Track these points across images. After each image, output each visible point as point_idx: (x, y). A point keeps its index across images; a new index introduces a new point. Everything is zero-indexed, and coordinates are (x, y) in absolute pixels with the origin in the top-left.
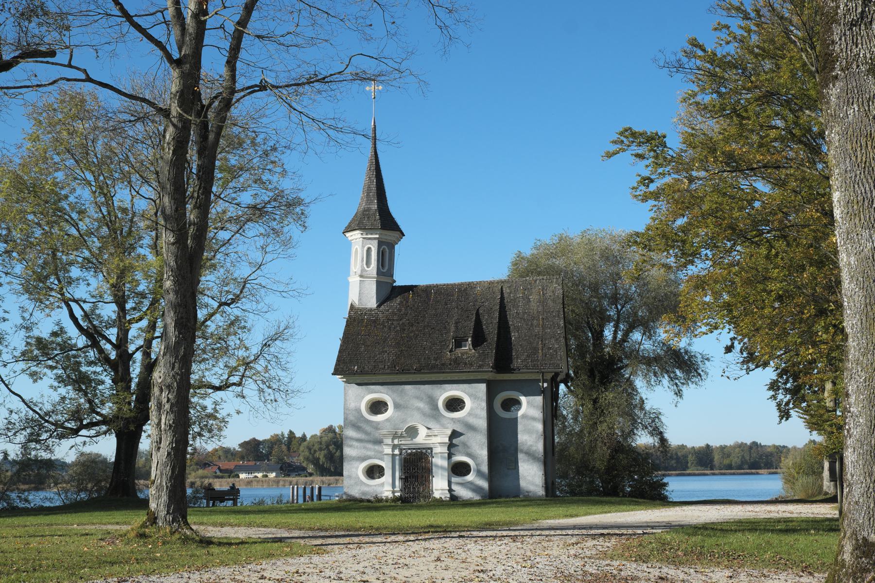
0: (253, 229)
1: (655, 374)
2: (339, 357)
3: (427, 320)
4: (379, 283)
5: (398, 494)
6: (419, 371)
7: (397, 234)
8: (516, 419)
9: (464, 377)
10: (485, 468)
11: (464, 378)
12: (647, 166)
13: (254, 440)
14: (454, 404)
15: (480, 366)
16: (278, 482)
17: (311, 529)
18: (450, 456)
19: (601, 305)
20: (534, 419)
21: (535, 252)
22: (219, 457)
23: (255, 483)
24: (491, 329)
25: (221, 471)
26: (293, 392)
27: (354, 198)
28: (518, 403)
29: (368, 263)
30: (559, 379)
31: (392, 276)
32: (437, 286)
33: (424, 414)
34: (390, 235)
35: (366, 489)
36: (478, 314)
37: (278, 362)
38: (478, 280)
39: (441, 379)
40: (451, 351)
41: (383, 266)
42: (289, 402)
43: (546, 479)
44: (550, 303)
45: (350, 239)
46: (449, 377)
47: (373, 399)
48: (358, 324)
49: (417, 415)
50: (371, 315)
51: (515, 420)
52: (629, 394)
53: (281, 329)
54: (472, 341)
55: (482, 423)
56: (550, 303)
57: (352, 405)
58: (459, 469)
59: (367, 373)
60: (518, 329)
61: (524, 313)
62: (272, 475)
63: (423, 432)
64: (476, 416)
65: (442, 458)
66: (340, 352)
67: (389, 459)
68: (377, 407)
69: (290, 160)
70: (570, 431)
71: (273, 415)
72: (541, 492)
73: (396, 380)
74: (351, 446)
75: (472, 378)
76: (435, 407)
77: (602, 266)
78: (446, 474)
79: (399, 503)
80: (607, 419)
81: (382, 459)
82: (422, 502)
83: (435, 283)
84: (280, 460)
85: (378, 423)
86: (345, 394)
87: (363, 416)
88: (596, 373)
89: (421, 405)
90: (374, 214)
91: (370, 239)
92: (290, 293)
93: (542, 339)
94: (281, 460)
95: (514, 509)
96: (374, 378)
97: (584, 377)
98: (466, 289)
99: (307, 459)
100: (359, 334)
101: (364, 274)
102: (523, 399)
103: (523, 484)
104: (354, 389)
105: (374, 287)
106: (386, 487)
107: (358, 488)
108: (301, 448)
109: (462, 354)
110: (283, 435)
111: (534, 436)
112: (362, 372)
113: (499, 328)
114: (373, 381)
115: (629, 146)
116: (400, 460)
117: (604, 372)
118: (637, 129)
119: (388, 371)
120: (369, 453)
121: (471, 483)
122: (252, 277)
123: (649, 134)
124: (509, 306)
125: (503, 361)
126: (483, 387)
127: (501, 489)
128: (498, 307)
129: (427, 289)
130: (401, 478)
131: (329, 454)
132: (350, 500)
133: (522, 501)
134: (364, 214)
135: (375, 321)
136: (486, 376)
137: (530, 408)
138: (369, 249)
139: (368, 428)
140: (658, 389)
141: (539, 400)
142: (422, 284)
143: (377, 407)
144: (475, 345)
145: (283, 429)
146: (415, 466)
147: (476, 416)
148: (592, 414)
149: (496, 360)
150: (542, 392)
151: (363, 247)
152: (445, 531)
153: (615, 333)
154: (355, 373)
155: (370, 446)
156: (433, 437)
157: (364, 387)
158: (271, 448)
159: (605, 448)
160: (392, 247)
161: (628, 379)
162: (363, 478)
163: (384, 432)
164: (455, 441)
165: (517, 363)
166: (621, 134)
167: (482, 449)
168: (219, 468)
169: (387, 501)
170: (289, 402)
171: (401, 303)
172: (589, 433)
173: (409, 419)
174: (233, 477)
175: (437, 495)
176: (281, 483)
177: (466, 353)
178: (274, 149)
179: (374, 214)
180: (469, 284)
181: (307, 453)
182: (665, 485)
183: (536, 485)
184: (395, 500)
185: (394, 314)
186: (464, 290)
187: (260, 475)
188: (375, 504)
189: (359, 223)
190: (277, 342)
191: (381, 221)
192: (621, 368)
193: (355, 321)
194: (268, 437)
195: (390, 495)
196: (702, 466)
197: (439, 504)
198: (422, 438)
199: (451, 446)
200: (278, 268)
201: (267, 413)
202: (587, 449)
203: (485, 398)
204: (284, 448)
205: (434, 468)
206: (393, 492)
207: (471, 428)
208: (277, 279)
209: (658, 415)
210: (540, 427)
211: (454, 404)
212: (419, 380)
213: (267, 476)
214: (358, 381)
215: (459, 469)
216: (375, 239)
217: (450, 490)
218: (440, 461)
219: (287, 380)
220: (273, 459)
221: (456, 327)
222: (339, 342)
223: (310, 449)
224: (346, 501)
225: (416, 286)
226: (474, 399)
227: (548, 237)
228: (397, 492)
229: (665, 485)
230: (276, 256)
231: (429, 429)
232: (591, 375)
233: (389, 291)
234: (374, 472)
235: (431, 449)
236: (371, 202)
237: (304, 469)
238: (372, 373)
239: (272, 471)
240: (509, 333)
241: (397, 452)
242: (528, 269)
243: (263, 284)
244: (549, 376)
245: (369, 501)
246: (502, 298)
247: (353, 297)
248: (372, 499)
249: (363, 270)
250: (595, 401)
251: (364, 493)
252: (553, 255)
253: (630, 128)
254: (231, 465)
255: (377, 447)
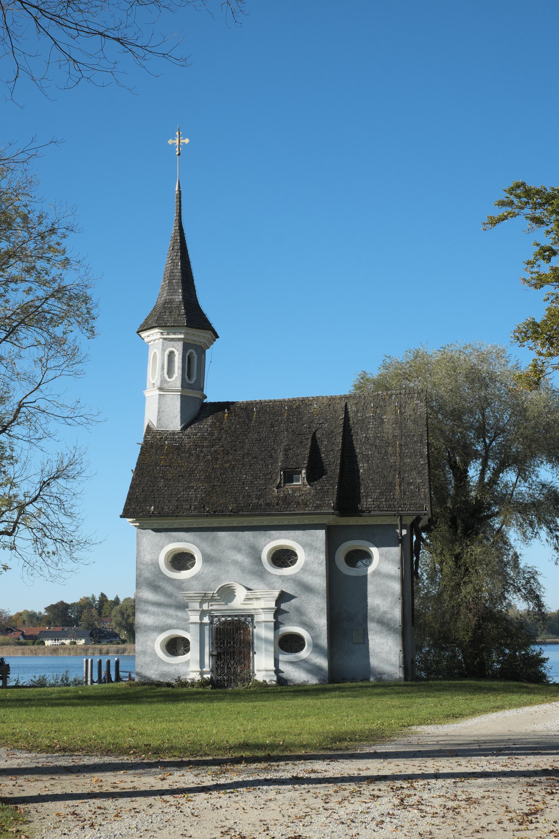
0: (28, 335)
1: (531, 525)
2: (129, 494)
3: (247, 446)
4: (184, 399)
5: (207, 676)
6: (235, 513)
7: (208, 334)
8: (366, 576)
9: (296, 521)
10: (324, 642)
11: (296, 523)
12: (548, 232)
13: (62, 603)
14: (283, 558)
15: (317, 507)
16: (87, 650)
17: (50, 749)
18: (277, 626)
19: (464, 436)
20: (390, 577)
21: (383, 371)
22: (24, 622)
23: (61, 651)
24: (332, 458)
25: (24, 637)
26: (79, 543)
27: (153, 286)
28: (368, 556)
29: (170, 372)
30: (420, 525)
31: (202, 389)
32: (261, 402)
33: (243, 569)
34: (199, 336)
35: (166, 669)
36: (314, 439)
37: (61, 505)
38: (315, 395)
39: (266, 523)
40: (278, 487)
41: (190, 377)
42: (74, 555)
43: (405, 657)
44: (410, 424)
45: (146, 340)
46: (276, 521)
47: (175, 550)
48: (155, 449)
49: (234, 571)
50: (173, 439)
51: (364, 579)
52: (499, 549)
53: (65, 464)
54: (307, 473)
55: (320, 582)
56: (410, 424)
57: (147, 558)
58: (289, 644)
59: (167, 515)
60: (367, 459)
61: (376, 438)
62: (82, 642)
63: (241, 593)
64: (313, 573)
65: (267, 627)
66: (131, 487)
67: (195, 629)
68: (181, 560)
69: (72, 245)
70: (426, 594)
71: (53, 571)
72: (399, 673)
73: (205, 525)
74: (146, 612)
75: (306, 522)
76: (258, 560)
77: (466, 390)
78: (272, 649)
79: (209, 688)
80: (473, 579)
81: (187, 630)
82: (240, 687)
83: (258, 399)
84: (90, 625)
85: (181, 582)
86: (138, 544)
87: (162, 573)
88: (459, 522)
89: (239, 557)
90: (178, 308)
91: (172, 340)
92: (77, 419)
93: (399, 476)
94: (91, 625)
95: (365, 700)
96: (177, 522)
97: (443, 528)
98: (298, 407)
99: (119, 624)
100: (157, 465)
101: (166, 386)
102: (374, 551)
103: (374, 662)
104: (150, 536)
105: (178, 403)
106: (192, 666)
107: (155, 667)
108: (113, 613)
109: (294, 491)
110: (93, 598)
111: (389, 599)
112: (161, 514)
113: (342, 457)
114: (175, 526)
115: (522, 208)
116: (211, 630)
117: (465, 520)
118: (533, 184)
119: (195, 513)
120: (170, 621)
121: (305, 661)
122: (29, 399)
123: (549, 191)
124: (355, 428)
125: (348, 501)
126: (322, 534)
127: (345, 671)
128: (341, 430)
129: (248, 407)
130: (211, 655)
131: (100, 622)
132: (143, 684)
133: (374, 686)
134: (164, 308)
135: (178, 448)
136: (326, 520)
137: (383, 564)
138: (171, 354)
139: (169, 588)
140: (535, 542)
141: (396, 551)
142: (240, 400)
143: (181, 560)
144: (311, 478)
145: (93, 591)
146: (230, 639)
147: (313, 573)
148: (454, 574)
149: (338, 499)
150: (400, 541)
151: (164, 350)
152: (268, 759)
153: (483, 472)
154: (151, 516)
155: (171, 612)
156: (254, 601)
157: (163, 534)
158: (81, 612)
159: (470, 616)
160: (201, 351)
161: (499, 530)
162: (161, 654)
163: (191, 593)
164: (283, 606)
165: (366, 503)
166: (511, 191)
167: (320, 617)
168: (23, 634)
169: (193, 684)
170: (74, 555)
171: (214, 423)
172: (451, 597)
173: (223, 577)
174: (38, 644)
175: (260, 677)
176: (90, 651)
177: (299, 490)
178: (52, 231)
179: (178, 308)
180: (303, 400)
181: (119, 618)
182: (544, 660)
183: (392, 665)
184: (204, 683)
185: (203, 438)
186: (297, 408)
187: (67, 642)
188: (172, 692)
189: (158, 320)
190: (60, 481)
191: (187, 316)
192: (489, 517)
193: (152, 447)
194: (77, 600)
195: (197, 677)
196: (553, 634)
197: (263, 690)
198: (239, 601)
199: (278, 612)
200: (61, 389)
201: (45, 569)
202: (448, 616)
203: (323, 548)
204: (94, 612)
205: (255, 641)
206: (202, 673)
207: (307, 589)
208: (61, 402)
209: (533, 575)
210: (396, 587)
211: (283, 558)
212: (235, 524)
213: (75, 643)
214: (156, 526)
215: (289, 644)
216: (179, 339)
217: (277, 671)
218: (263, 632)
219: (72, 528)
220: (83, 624)
221: (286, 455)
222: (131, 475)
223: (122, 614)
224: (138, 684)
225: (233, 403)
226: (309, 551)
227: (400, 355)
228: (206, 673)
229: (544, 660)
230: (59, 373)
231: (249, 589)
232: (453, 525)
233: (198, 410)
234: (176, 646)
235: (252, 616)
236: (174, 292)
237: (116, 636)
238: (174, 514)
239: (81, 637)
240: (355, 463)
241: (206, 620)
242: (378, 392)
243: (43, 407)
244: (408, 521)
245: (169, 685)
246: (347, 418)
247: (151, 416)
248: (173, 682)
249: (163, 381)
250: (457, 557)
251: (164, 675)
252: (407, 377)
253: (523, 184)
254: (35, 631)
255: (179, 614)
